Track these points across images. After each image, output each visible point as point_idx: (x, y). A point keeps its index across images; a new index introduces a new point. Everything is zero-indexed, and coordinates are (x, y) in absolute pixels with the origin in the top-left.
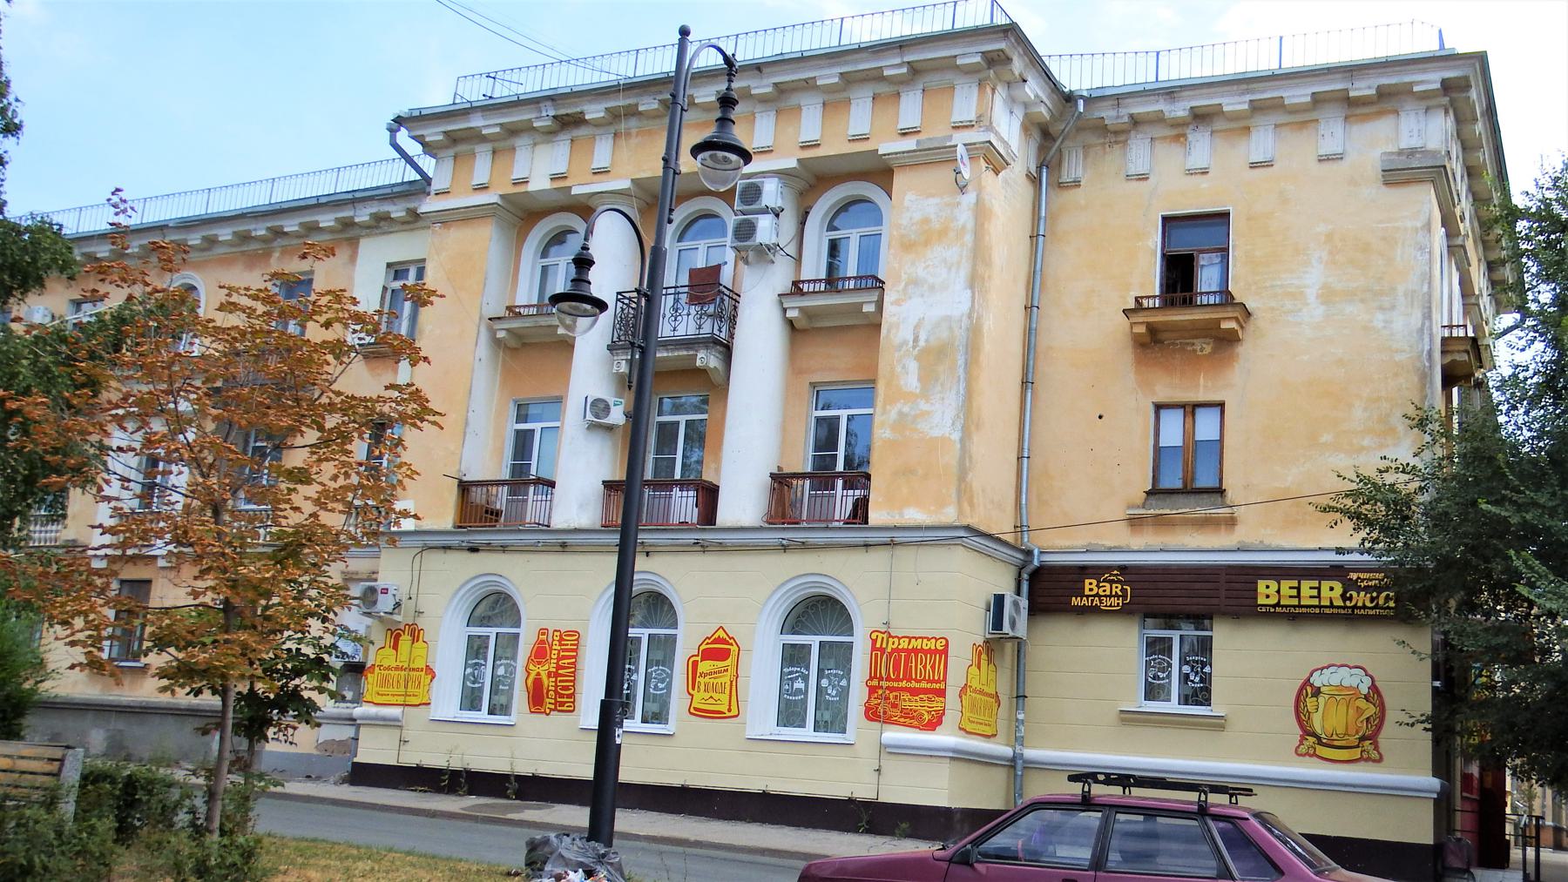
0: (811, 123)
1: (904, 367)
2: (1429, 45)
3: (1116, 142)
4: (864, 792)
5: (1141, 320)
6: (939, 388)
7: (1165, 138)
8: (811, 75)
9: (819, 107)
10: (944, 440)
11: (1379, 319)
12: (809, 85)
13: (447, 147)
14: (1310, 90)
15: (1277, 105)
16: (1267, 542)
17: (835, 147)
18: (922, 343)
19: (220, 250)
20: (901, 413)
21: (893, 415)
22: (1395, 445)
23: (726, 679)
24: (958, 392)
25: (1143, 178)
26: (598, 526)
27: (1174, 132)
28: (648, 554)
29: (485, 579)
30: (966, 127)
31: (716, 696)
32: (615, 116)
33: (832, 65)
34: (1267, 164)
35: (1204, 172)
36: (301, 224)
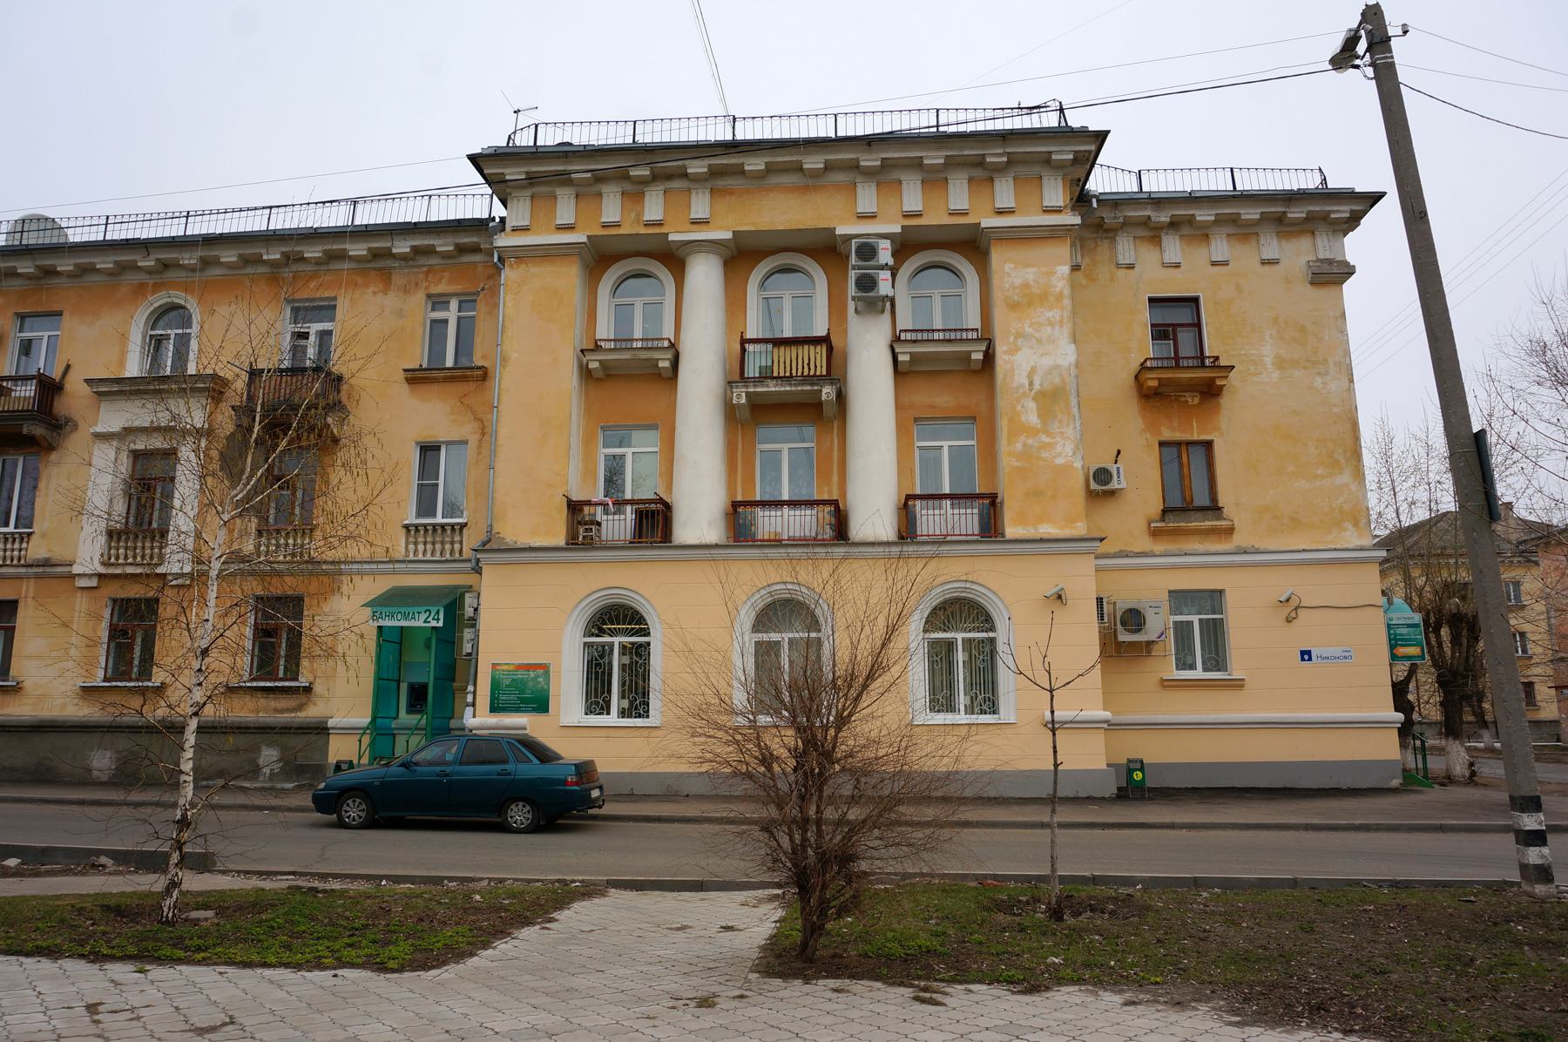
0: (912, 196)
1: (1023, 406)
2: (1311, 182)
3: (1106, 238)
5: (1155, 376)
6: (1058, 424)
7: (1144, 237)
9: (919, 183)
10: (1067, 467)
11: (1319, 381)
12: (918, 164)
13: (524, 187)
14: (1259, 211)
15: (1234, 220)
16: (1257, 546)
17: (936, 218)
18: (1037, 386)
19: (215, 271)
20: (1025, 445)
21: (1019, 446)
22: (1340, 473)
24: (1075, 428)
25: (1131, 267)
26: (723, 541)
27: (1151, 234)
30: (1055, 211)
32: (715, 173)
34: (1225, 263)
35: (1177, 266)
36: (324, 251)
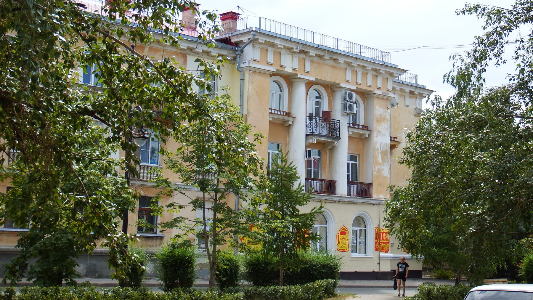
4: (376, 269)
8: (365, 65)
10: (386, 177)
18: (381, 150)
20: (378, 168)
23: (346, 241)
28: (326, 203)
29: (363, 212)
31: (344, 245)
33: (371, 65)
